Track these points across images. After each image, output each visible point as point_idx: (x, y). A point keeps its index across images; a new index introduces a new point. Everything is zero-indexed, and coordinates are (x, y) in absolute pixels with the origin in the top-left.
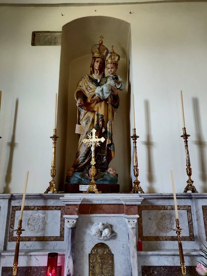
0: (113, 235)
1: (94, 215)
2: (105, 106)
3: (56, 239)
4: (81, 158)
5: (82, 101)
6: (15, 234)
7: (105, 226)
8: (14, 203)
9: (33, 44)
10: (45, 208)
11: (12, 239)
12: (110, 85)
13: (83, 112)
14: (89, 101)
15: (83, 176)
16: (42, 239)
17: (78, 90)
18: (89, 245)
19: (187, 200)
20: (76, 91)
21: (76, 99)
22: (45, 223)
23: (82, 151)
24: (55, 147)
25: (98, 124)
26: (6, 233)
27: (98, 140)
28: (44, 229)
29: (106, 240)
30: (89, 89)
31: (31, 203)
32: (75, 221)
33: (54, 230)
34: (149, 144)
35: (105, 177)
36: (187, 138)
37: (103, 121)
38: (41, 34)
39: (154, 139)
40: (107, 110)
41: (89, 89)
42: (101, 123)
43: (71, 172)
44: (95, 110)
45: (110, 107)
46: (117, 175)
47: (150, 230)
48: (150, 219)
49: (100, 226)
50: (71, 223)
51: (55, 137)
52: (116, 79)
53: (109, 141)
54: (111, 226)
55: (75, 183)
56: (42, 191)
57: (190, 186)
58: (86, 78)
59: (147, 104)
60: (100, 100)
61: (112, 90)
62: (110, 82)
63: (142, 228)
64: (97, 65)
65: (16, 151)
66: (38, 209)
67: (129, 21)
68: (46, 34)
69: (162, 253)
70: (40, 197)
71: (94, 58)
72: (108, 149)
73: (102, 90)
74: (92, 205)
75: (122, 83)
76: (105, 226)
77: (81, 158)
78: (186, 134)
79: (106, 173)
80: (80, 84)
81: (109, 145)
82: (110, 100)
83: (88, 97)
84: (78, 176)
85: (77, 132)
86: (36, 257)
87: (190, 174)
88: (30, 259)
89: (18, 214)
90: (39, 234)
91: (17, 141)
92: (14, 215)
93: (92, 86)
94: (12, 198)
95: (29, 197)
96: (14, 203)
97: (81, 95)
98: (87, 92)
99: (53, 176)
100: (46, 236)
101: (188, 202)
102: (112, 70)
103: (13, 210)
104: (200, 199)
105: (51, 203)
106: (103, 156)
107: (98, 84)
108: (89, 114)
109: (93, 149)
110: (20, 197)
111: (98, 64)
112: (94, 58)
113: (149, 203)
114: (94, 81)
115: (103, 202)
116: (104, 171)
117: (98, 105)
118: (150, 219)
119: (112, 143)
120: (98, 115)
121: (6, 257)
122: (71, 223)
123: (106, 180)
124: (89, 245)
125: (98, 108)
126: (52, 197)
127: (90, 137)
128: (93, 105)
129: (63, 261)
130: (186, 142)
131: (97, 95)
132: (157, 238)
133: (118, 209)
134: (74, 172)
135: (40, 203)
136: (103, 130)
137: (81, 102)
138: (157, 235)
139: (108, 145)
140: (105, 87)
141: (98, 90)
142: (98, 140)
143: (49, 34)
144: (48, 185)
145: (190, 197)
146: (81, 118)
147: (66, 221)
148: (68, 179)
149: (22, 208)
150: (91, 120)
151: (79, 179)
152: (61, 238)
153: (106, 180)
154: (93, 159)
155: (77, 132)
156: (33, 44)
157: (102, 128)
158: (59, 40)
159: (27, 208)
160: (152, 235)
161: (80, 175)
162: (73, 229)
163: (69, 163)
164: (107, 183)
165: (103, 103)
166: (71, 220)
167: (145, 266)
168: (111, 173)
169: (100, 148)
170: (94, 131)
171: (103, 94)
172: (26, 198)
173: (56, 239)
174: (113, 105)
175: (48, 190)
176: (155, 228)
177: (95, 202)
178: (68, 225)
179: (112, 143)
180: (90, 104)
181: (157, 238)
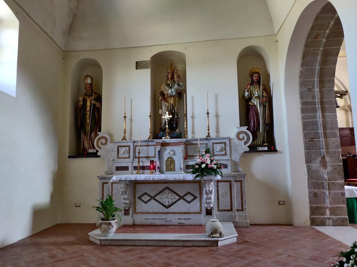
0: (175, 154)
1: (167, 147)
2: (174, 99)
3: (153, 157)
4: (163, 125)
5: (162, 98)
6: (137, 155)
7: (171, 151)
8: (135, 144)
9: (137, 69)
10: (148, 146)
11: (136, 158)
12: (175, 88)
13: (163, 102)
14: (166, 97)
15: (164, 133)
16: (147, 157)
17: (160, 91)
18: (165, 158)
19: (206, 141)
20: (159, 92)
21: (159, 96)
22: (148, 151)
23: (163, 122)
24: (150, 121)
25: (170, 108)
26: (133, 155)
27: (169, 117)
28: (148, 154)
29: (172, 156)
30: (166, 90)
31: (142, 144)
32: (160, 149)
33: (152, 154)
34: (193, 117)
35: (174, 133)
36: (208, 114)
37: (173, 107)
38: (140, 62)
39: (195, 115)
40: (175, 101)
41: (166, 90)
42: (172, 108)
43: (159, 132)
44: (169, 101)
45: (177, 99)
46: (181, 133)
47: (191, 153)
48: (191, 149)
49: (169, 151)
50: (158, 149)
51: (150, 116)
52: (179, 85)
53: (338, 87)
54: (174, 151)
55: (160, 136)
56: (147, 139)
57: (209, 136)
58: (164, 84)
59: (193, 98)
60: (171, 96)
61: (176, 91)
62: (176, 86)
63: (187, 153)
64: (170, 76)
65: (133, 123)
66: (145, 146)
67: (184, 53)
68: (143, 62)
69: (193, 160)
70: (146, 141)
71: (168, 73)
72: (176, 120)
73: (172, 91)
74: (167, 143)
75: (182, 86)
76: (171, 151)
77: (163, 125)
78: (208, 112)
79: (175, 132)
80: (161, 87)
81: (177, 118)
82: (176, 95)
83: (165, 94)
84: (162, 133)
85: (160, 113)
86: (146, 163)
87: (209, 130)
88: (144, 163)
89: (137, 148)
90: (146, 156)
91: (133, 118)
92: (135, 149)
93: (167, 88)
94: (134, 142)
95: (141, 141)
96: (135, 144)
97: (162, 94)
98: (165, 92)
99: (150, 133)
100: (150, 156)
101: (207, 142)
102: (177, 79)
103: (135, 147)
104: (211, 140)
105: (150, 143)
106: (174, 124)
107: (171, 88)
108: (166, 103)
109: (167, 121)
110: (138, 142)
111: (170, 76)
112: (168, 73)
113: (190, 142)
114: (168, 85)
115: (171, 142)
116: (174, 131)
117: (170, 98)
118: (191, 149)
119: (178, 117)
120: (170, 104)
121: (135, 163)
122: (158, 149)
123: (174, 135)
124: (165, 158)
125: (170, 100)
126: (151, 141)
127: (165, 115)
128: (168, 99)
129: (156, 164)
130: (208, 116)
131: (169, 94)
132: (193, 156)
133: (177, 144)
134: (160, 132)
135: (146, 144)
136: (173, 111)
137: (161, 98)
138: (193, 155)
139: (176, 118)
140: (173, 90)
141: (170, 91)
142: (169, 117)
143: (144, 62)
144: (149, 137)
145: (207, 140)
146: (162, 105)
147: (156, 148)
148: (157, 134)
149: (139, 146)
150: (167, 106)
151: (162, 135)
152: (155, 157)
153: (174, 135)
154: (167, 125)
155: (160, 113)
156: (137, 69)
157: (173, 110)
158: (149, 65)
159: (141, 146)
160: (191, 155)
161: (163, 133)
162: (159, 152)
163: (158, 129)
164: (175, 136)
165: (173, 97)
166: (158, 148)
167: (187, 165)
168: (177, 132)
169: (170, 121)
170: (167, 113)
171: (172, 93)
172: (140, 142)
173: (153, 157)
174: (179, 97)
175: (149, 139)
176: (192, 152)
177: (168, 142)
178: (157, 150)
179: (178, 117)
180: (166, 98)
181: (193, 156)
